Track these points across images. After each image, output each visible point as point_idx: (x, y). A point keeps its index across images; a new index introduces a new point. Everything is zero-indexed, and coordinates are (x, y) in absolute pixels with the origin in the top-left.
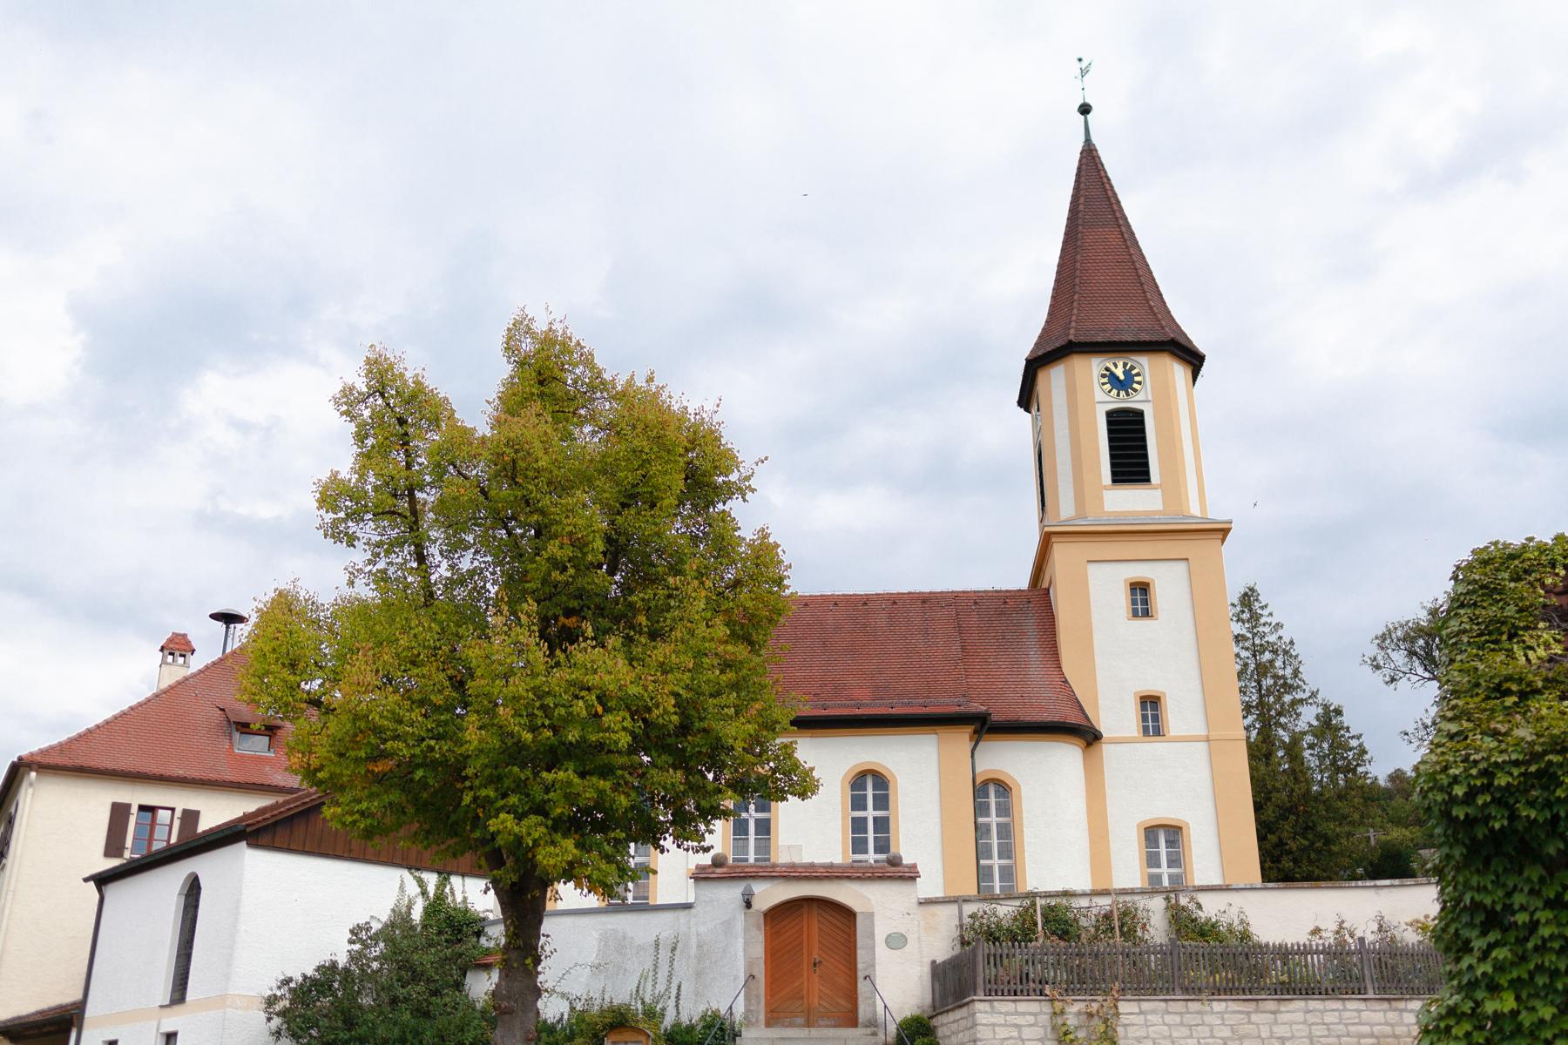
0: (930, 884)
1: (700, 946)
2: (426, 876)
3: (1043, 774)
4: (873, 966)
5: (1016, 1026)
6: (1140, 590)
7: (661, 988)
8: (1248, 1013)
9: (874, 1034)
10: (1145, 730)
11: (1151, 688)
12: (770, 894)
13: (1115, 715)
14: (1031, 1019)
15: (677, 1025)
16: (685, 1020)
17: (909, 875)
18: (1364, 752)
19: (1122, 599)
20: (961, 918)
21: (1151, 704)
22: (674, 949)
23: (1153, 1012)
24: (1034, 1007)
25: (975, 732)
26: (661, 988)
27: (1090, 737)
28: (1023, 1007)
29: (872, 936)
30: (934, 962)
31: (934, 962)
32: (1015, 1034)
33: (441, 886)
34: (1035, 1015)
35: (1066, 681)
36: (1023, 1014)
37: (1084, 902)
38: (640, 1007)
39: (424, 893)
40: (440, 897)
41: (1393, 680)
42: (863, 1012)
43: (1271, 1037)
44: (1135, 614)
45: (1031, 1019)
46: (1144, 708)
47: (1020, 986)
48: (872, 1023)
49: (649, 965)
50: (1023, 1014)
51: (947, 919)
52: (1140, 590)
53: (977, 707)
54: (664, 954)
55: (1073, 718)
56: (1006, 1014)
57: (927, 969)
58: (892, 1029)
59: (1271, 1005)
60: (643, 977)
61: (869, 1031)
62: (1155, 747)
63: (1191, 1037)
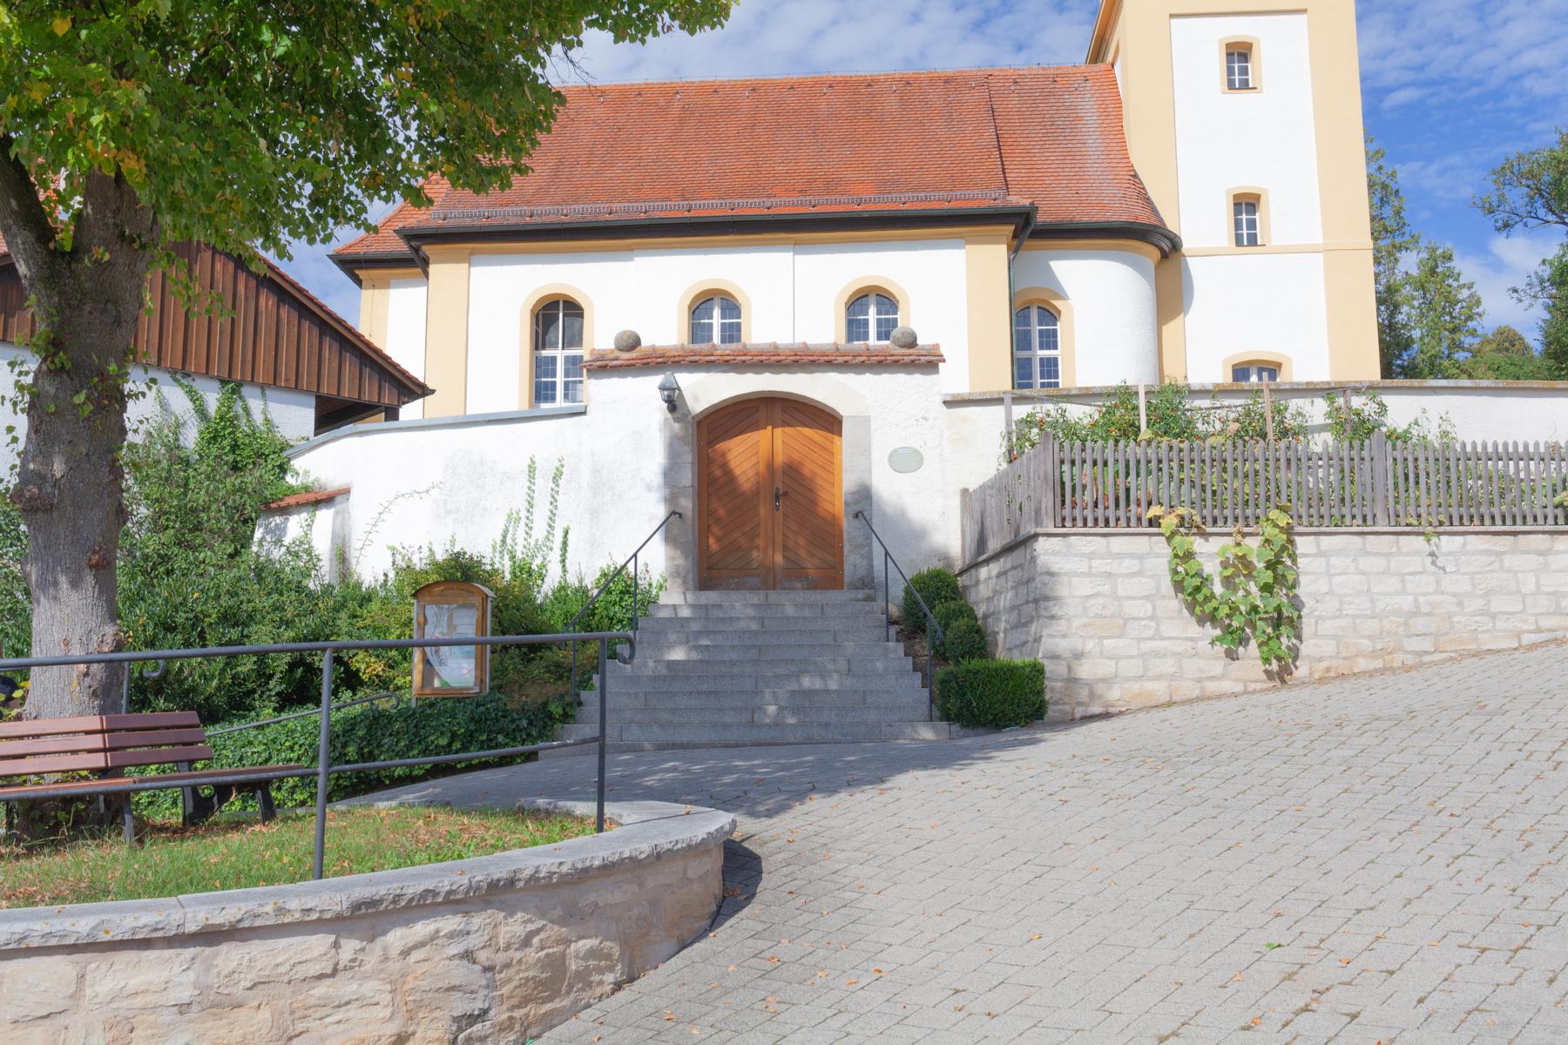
0: (954, 377)
1: (596, 471)
2: (200, 384)
3: (1098, 296)
4: (870, 469)
5: (1109, 575)
6: (1239, 54)
7: (539, 532)
8: (1500, 554)
9: (869, 599)
10: (1239, 242)
11: (1246, 184)
12: (706, 390)
13: (1199, 222)
14: (1134, 565)
15: (563, 588)
16: (573, 580)
17: (929, 363)
18: (1478, 303)
19: (1216, 63)
20: (1008, 424)
21: (1246, 204)
22: (556, 478)
23: (1341, 552)
24: (1140, 544)
25: (1015, 236)
26: (539, 532)
27: (1166, 246)
28: (1117, 544)
29: (867, 451)
30: (965, 492)
31: (965, 492)
32: (1106, 588)
33: (227, 403)
34: (1141, 557)
35: (1135, 176)
36: (1121, 556)
37: (1205, 403)
38: (507, 563)
39: (202, 412)
40: (227, 420)
41: (1506, 225)
42: (852, 563)
43: (1538, 592)
44: (1231, 85)
45: (1134, 565)
46: (1237, 212)
47: (1117, 511)
48: (867, 584)
49: (520, 504)
50: (1121, 556)
51: (992, 421)
52: (1239, 54)
53: (1017, 200)
54: (543, 485)
55: (1144, 218)
56: (1091, 556)
57: (955, 502)
58: (898, 591)
59: (1540, 541)
60: (513, 519)
61: (861, 594)
62: (1249, 259)
63: (1403, 592)
